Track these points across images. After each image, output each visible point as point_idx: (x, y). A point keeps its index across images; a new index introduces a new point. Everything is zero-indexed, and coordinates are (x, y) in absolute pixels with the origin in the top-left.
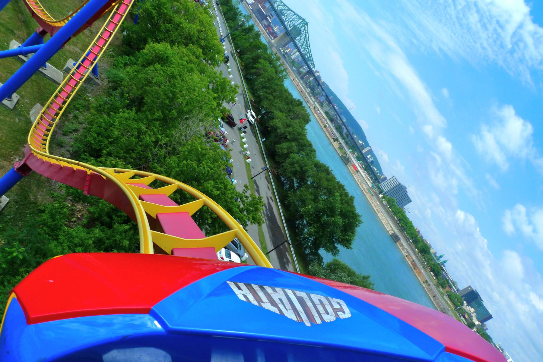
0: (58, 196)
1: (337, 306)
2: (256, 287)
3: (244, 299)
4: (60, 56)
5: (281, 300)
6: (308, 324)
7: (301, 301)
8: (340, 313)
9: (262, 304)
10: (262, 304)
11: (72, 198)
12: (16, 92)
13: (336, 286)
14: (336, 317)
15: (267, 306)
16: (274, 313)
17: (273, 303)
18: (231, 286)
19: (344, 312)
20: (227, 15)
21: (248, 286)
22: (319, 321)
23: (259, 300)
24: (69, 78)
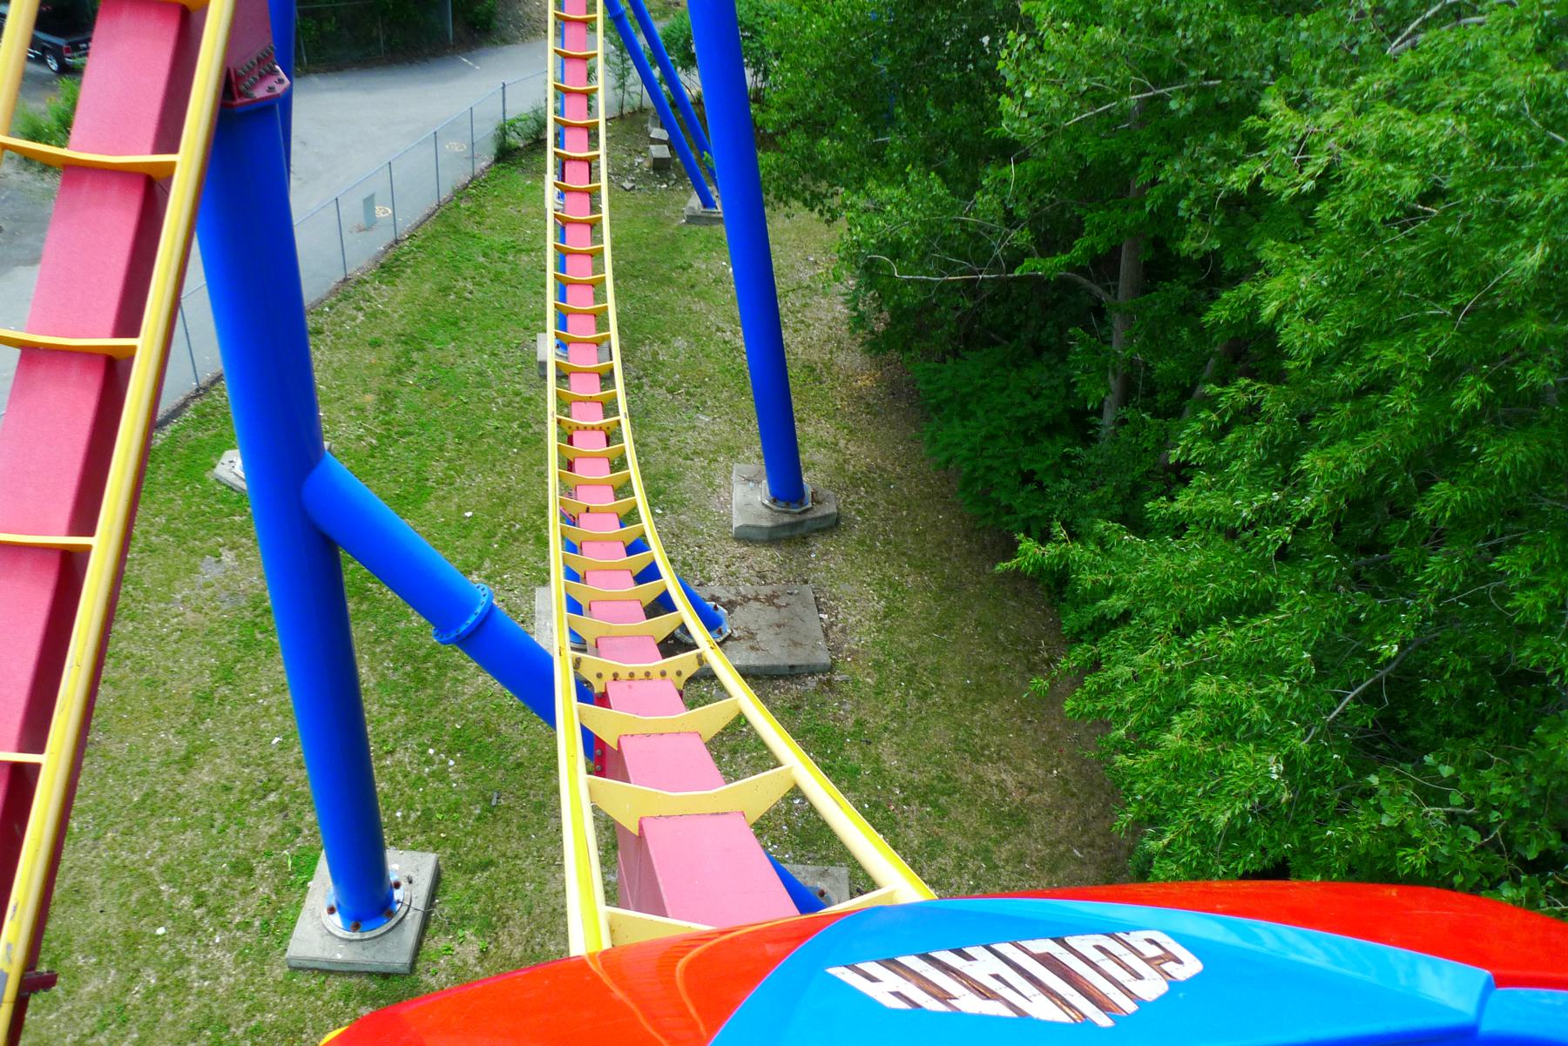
0: (1519, 62)
1: (1153, 951)
2: (1005, 949)
3: (902, 1005)
4: (114, 684)
5: (997, 977)
6: (1103, 1020)
7: (1047, 960)
8: (1169, 967)
9: (953, 1002)
10: (953, 1002)
11: (1204, 323)
12: (224, 395)
13: (791, 951)
14: (1169, 983)
15: (969, 1003)
16: (998, 1019)
17: (985, 993)
18: (840, 976)
19: (1179, 962)
20: (537, 456)
21: (891, 964)
22: (1129, 1006)
23: (943, 996)
24: (555, 167)
